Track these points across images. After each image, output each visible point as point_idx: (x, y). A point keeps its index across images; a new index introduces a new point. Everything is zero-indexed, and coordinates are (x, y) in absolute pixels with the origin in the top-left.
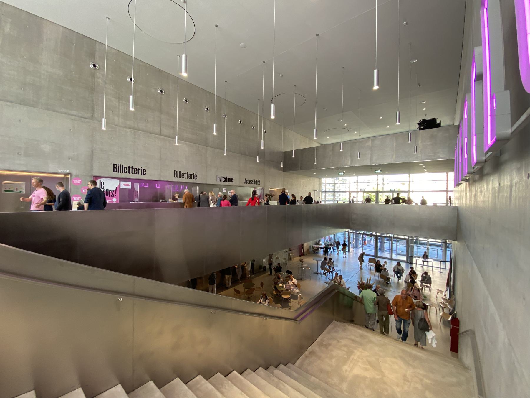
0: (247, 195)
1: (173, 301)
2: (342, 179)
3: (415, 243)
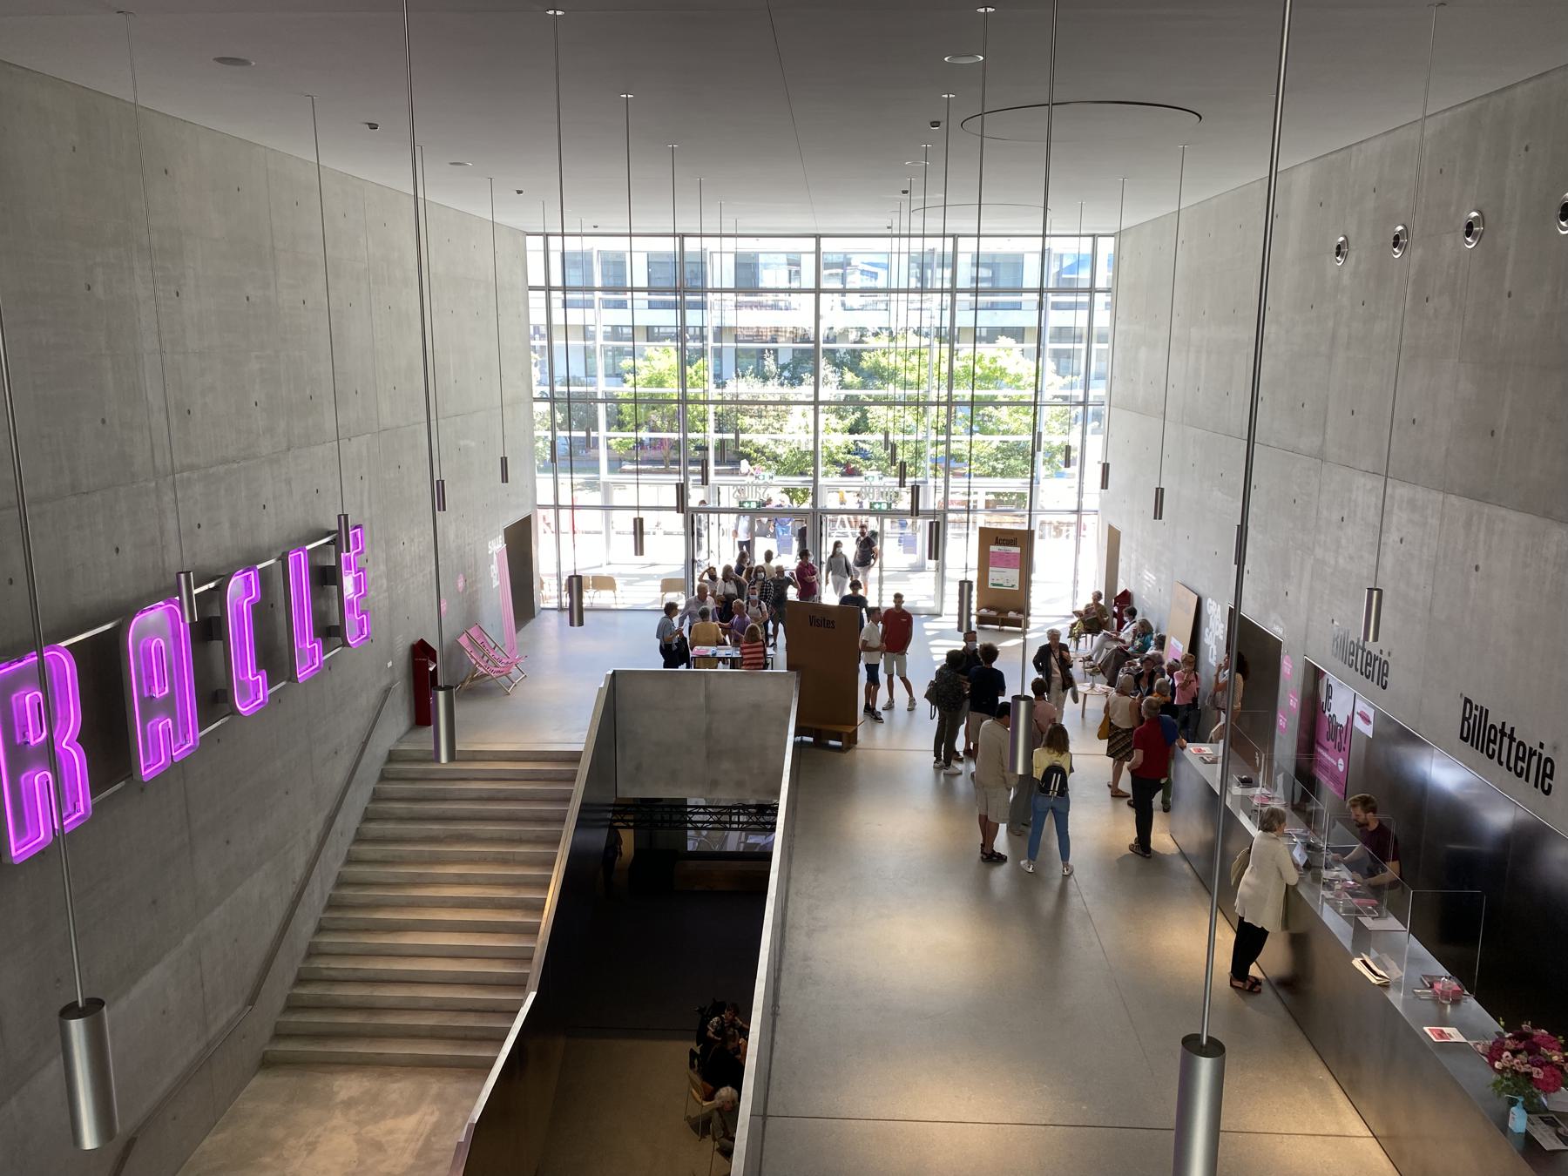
2: (875, 275)
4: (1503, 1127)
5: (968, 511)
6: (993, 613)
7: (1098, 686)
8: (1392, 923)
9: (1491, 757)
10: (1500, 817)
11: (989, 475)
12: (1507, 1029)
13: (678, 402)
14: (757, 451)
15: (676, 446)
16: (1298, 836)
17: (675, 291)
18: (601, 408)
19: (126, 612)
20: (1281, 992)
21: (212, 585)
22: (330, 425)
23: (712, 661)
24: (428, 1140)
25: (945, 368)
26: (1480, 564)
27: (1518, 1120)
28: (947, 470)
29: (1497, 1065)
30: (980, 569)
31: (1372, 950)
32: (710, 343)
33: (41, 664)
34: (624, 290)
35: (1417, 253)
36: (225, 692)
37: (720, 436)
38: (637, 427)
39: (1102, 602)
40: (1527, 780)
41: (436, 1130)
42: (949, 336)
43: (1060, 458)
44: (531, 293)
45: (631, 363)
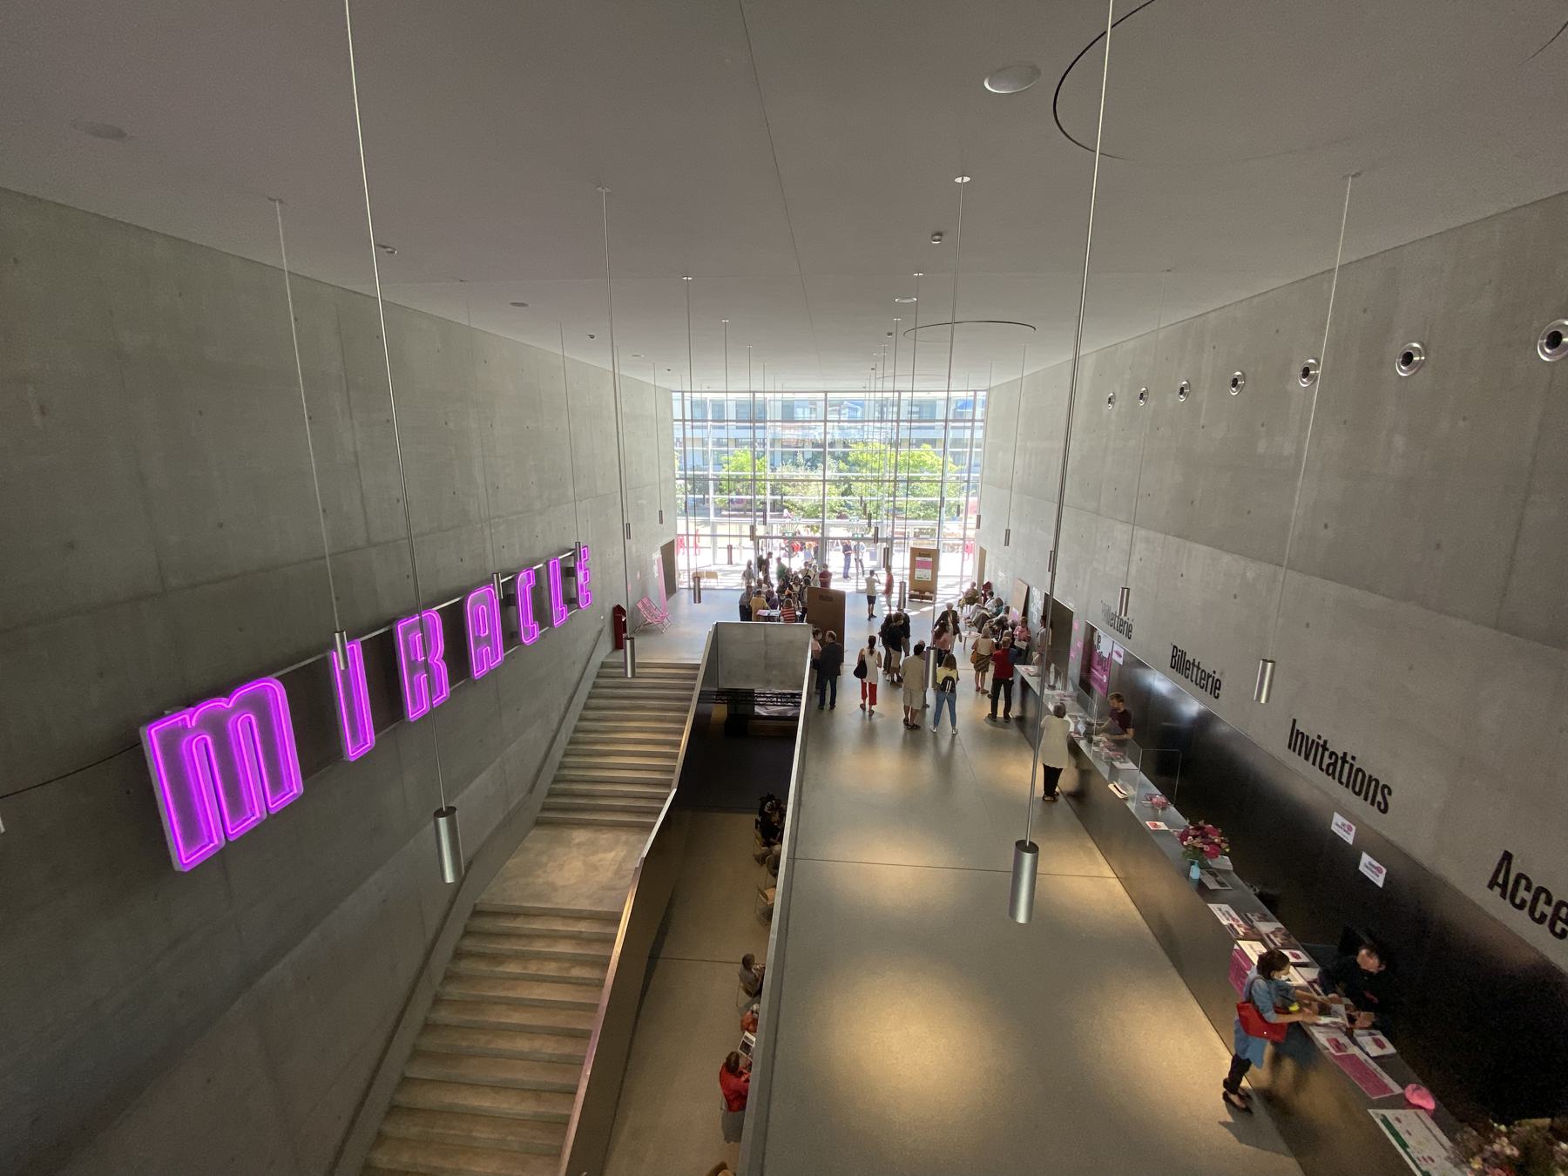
0: (1392, 1091)
1: (653, 958)
3: (803, 540)
4: (1188, 877)
5: (905, 538)
6: (918, 593)
7: (973, 633)
8: (1130, 765)
9: (1187, 677)
10: (1191, 707)
11: (916, 519)
12: (1191, 823)
13: (751, 480)
14: (792, 505)
15: (750, 502)
16: (1080, 717)
17: (750, 422)
18: (711, 483)
19: (465, 592)
20: (1069, 799)
21: (510, 577)
22: (570, 492)
23: (769, 618)
24: (620, 864)
25: (893, 461)
26: (1184, 573)
27: (1195, 873)
28: (894, 515)
29: (1185, 843)
30: (910, 569)
31: (1120, 780)
32: (768, 448)
33: (421, 620)
34: (723, 421)
35: (1152, 404)
36: (517, 632)
37: (773, 497)
38: (730, 492)
39: (976, 588)
40: (1206, 690)
41: (624, 860)
42: (896, 444)
43: (954, 509)
44: (675, 423)
45: (726, 457)
